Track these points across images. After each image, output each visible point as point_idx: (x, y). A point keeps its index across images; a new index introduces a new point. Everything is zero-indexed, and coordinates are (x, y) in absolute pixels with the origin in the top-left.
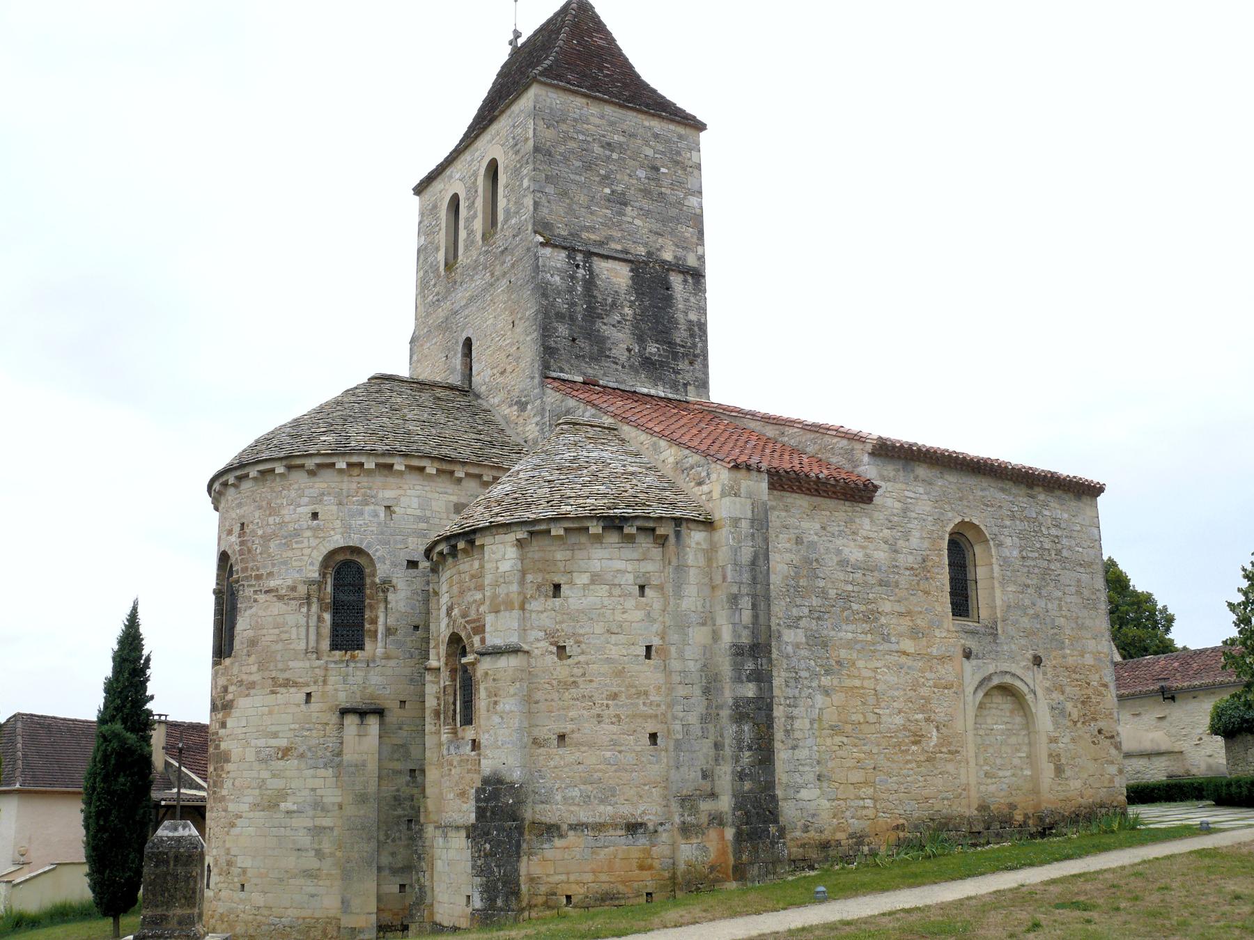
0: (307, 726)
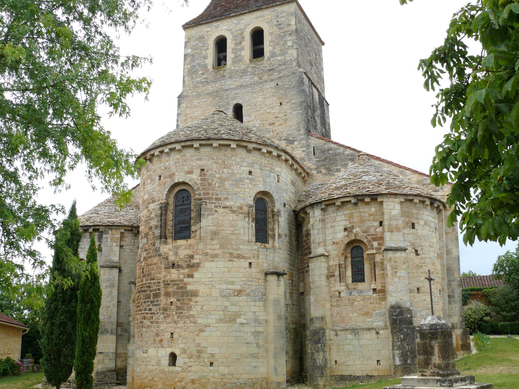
0: (250, 279)
